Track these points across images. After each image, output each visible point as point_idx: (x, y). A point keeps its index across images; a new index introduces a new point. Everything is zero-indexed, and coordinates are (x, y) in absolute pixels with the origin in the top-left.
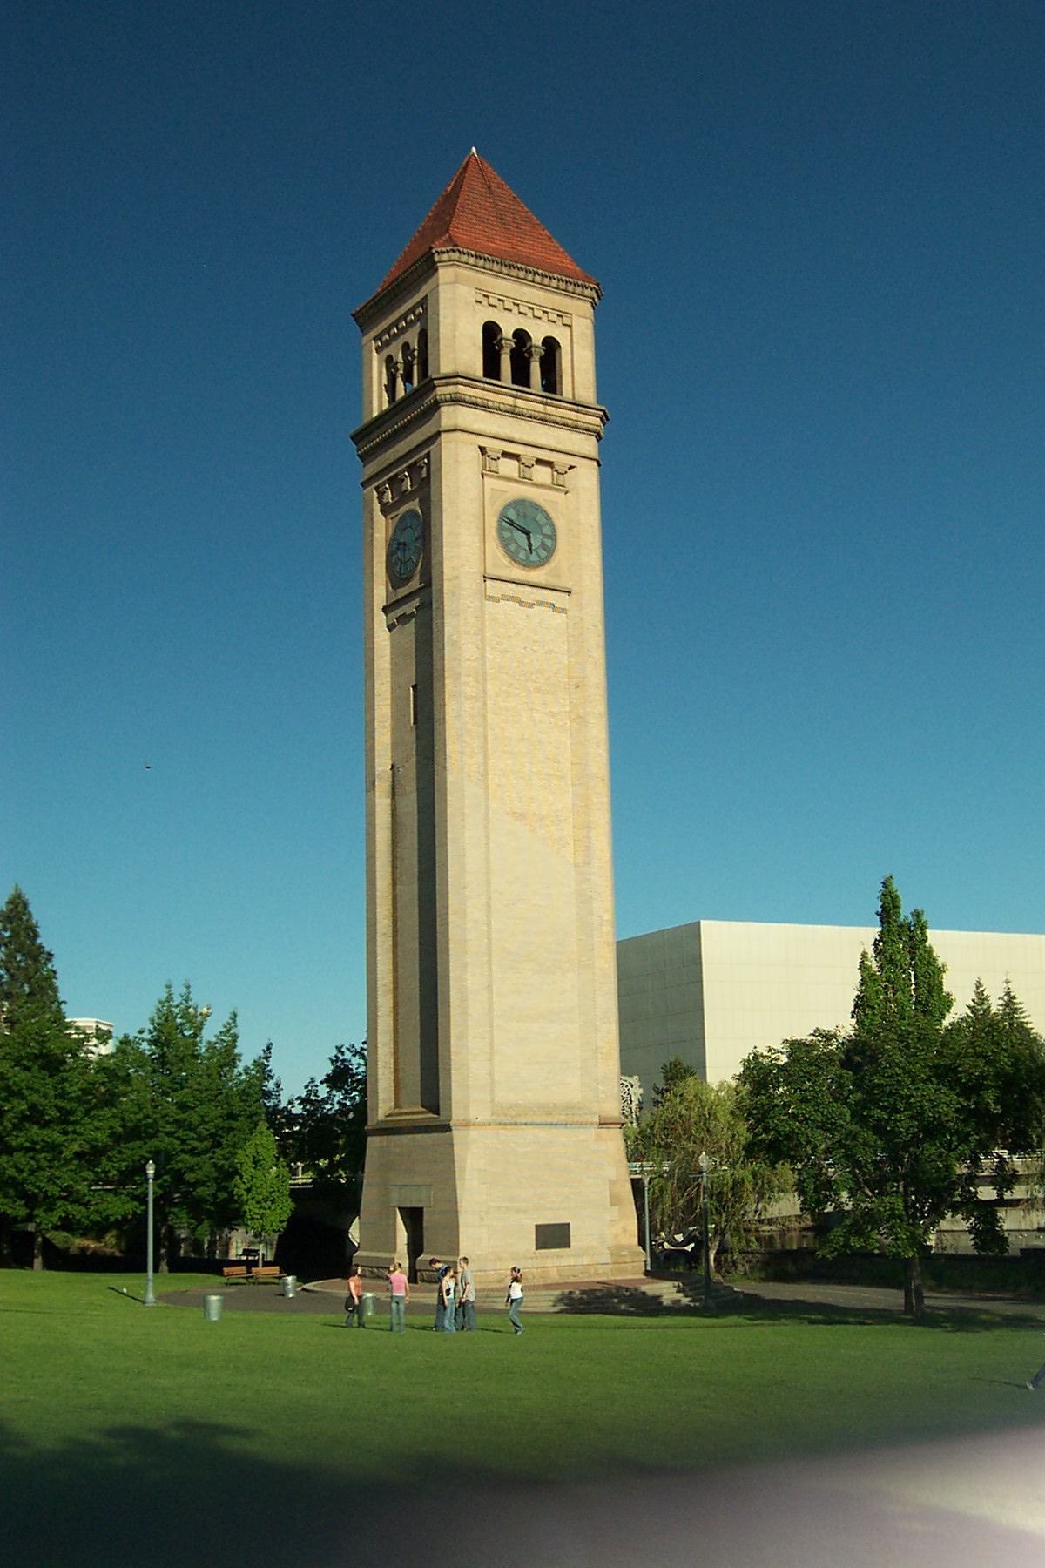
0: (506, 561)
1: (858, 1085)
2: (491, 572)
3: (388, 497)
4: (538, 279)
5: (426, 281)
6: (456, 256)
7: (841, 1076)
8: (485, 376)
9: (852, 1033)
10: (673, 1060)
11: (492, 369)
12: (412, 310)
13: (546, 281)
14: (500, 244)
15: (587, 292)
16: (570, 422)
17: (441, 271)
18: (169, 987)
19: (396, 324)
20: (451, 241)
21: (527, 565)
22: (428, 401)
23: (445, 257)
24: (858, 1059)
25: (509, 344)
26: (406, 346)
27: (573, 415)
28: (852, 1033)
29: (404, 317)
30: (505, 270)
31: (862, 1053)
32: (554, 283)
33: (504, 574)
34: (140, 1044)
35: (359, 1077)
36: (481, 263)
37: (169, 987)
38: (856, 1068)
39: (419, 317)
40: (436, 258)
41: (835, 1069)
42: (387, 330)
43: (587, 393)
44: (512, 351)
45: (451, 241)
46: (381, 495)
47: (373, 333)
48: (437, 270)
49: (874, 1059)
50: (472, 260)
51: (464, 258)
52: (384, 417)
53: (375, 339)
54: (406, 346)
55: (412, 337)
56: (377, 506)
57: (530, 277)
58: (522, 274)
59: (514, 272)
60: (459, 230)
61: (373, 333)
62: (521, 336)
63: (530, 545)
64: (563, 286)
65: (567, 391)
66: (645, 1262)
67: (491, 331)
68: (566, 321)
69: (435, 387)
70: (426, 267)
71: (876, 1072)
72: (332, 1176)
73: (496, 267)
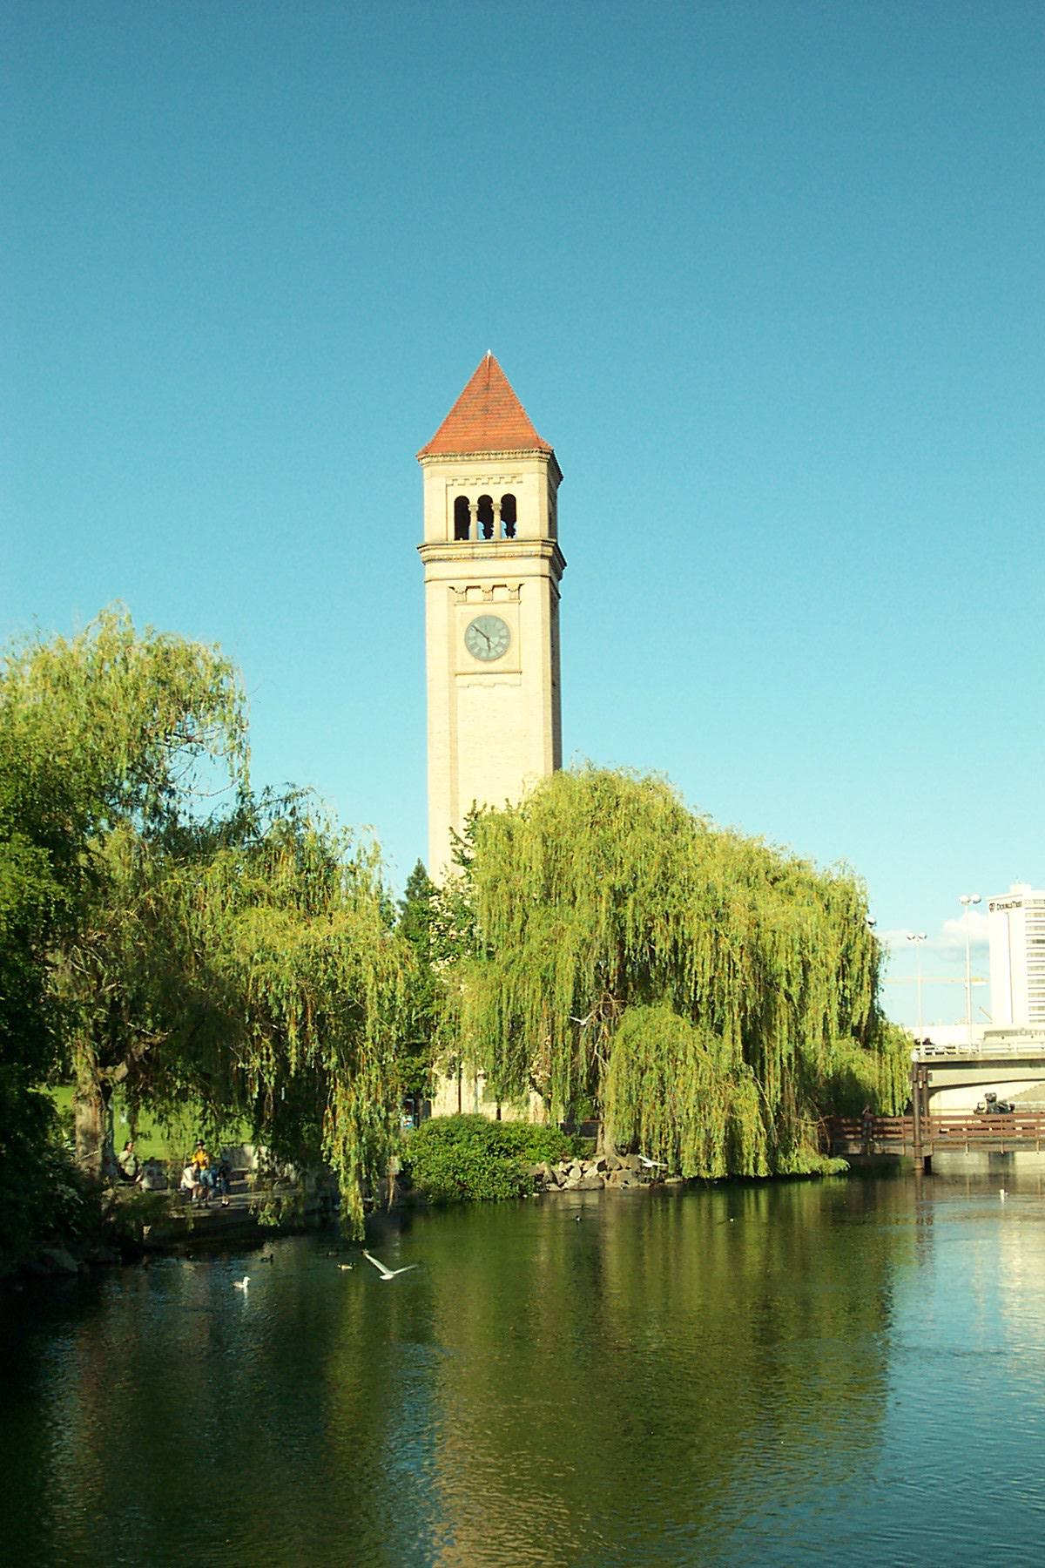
0: (472, 660)
2: (459, 669)
4: (492, 457)
10: (254, 908)
11: (462, 531)
13: (500, 456)
18: (507, 800)
21: (487, 660)
32: (506, 456)
33: (471, 669)
34: (780, 855)
35: (832, 1099)
36: (448, 458)
37: (507, 800)
50: (441, 459)
51: (435, 459)
58: (480, 457)
62: (485, 501)
63: (489, 647)
66: (805, 1334)
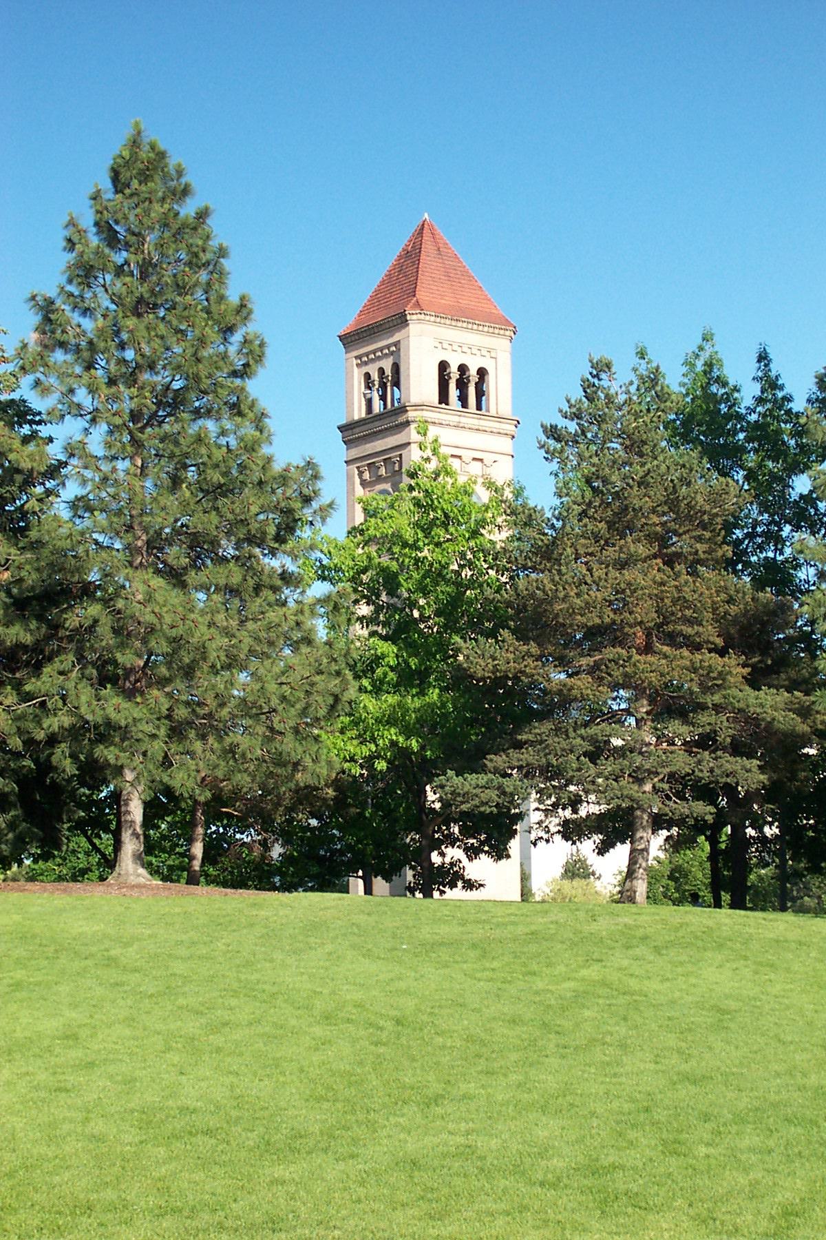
1: (677, 890)
3: (367, 476)
5: (399, 330)
6: (422, 317)
7: (668, 885)
8: (440, 403)
9: (548, 891)
11: (444, 397)
12: (388, 347)
13: (481, 328)
14: (448, 301)
15: (508, 333)
16: (495, 430)
17: (411, 326)
19: (374, 352)
20: (418, 305)
22: (402, 419)
23: (414, 317)
24: (677, 875)
25: (455, 375)
26: (381, 371)
27: (497, 425)
28: (548, 891)
29: (381, 349)
30: (454, 323)
31: (680, 872)
32: (486, 329)
36: (438, 320)
38: (676, 880)
39: (392, 353)
40: (409, 317)
41: (665, 881)
42: (367, 355)
43: (505, 407)
44: (457, 380)
45: (418, 305)
46: (361, 474)
47: (356, 353)
48: (408, 325)
49: (686, 876)
50: (433, 319)
51: (428, 318)
52: (361, 422)
53: (356, 357)
54: (381, 371)
55: (387, 365)
56: (357, 481)
57: (470, 326)
59: (460, 324)
60: (422, 294)
61: (356, 353)
64: (491, 330)
65: (493, 412)
67: (443, 366)
68: (493, 354)
69: (407, 411)
70: (401, 321)
71: (686, 883)
72: (763, 840)
73: (448, 322)
